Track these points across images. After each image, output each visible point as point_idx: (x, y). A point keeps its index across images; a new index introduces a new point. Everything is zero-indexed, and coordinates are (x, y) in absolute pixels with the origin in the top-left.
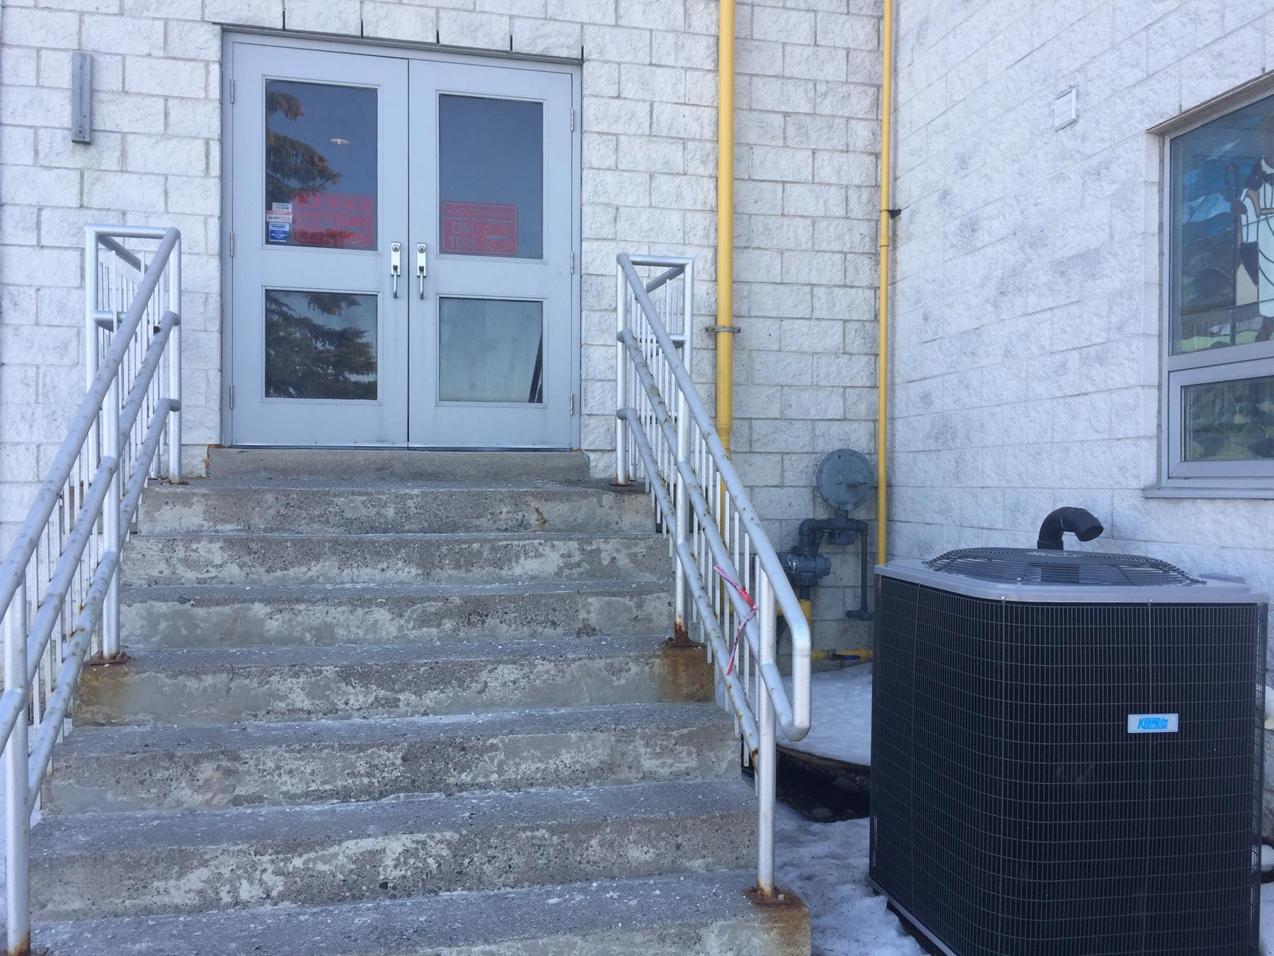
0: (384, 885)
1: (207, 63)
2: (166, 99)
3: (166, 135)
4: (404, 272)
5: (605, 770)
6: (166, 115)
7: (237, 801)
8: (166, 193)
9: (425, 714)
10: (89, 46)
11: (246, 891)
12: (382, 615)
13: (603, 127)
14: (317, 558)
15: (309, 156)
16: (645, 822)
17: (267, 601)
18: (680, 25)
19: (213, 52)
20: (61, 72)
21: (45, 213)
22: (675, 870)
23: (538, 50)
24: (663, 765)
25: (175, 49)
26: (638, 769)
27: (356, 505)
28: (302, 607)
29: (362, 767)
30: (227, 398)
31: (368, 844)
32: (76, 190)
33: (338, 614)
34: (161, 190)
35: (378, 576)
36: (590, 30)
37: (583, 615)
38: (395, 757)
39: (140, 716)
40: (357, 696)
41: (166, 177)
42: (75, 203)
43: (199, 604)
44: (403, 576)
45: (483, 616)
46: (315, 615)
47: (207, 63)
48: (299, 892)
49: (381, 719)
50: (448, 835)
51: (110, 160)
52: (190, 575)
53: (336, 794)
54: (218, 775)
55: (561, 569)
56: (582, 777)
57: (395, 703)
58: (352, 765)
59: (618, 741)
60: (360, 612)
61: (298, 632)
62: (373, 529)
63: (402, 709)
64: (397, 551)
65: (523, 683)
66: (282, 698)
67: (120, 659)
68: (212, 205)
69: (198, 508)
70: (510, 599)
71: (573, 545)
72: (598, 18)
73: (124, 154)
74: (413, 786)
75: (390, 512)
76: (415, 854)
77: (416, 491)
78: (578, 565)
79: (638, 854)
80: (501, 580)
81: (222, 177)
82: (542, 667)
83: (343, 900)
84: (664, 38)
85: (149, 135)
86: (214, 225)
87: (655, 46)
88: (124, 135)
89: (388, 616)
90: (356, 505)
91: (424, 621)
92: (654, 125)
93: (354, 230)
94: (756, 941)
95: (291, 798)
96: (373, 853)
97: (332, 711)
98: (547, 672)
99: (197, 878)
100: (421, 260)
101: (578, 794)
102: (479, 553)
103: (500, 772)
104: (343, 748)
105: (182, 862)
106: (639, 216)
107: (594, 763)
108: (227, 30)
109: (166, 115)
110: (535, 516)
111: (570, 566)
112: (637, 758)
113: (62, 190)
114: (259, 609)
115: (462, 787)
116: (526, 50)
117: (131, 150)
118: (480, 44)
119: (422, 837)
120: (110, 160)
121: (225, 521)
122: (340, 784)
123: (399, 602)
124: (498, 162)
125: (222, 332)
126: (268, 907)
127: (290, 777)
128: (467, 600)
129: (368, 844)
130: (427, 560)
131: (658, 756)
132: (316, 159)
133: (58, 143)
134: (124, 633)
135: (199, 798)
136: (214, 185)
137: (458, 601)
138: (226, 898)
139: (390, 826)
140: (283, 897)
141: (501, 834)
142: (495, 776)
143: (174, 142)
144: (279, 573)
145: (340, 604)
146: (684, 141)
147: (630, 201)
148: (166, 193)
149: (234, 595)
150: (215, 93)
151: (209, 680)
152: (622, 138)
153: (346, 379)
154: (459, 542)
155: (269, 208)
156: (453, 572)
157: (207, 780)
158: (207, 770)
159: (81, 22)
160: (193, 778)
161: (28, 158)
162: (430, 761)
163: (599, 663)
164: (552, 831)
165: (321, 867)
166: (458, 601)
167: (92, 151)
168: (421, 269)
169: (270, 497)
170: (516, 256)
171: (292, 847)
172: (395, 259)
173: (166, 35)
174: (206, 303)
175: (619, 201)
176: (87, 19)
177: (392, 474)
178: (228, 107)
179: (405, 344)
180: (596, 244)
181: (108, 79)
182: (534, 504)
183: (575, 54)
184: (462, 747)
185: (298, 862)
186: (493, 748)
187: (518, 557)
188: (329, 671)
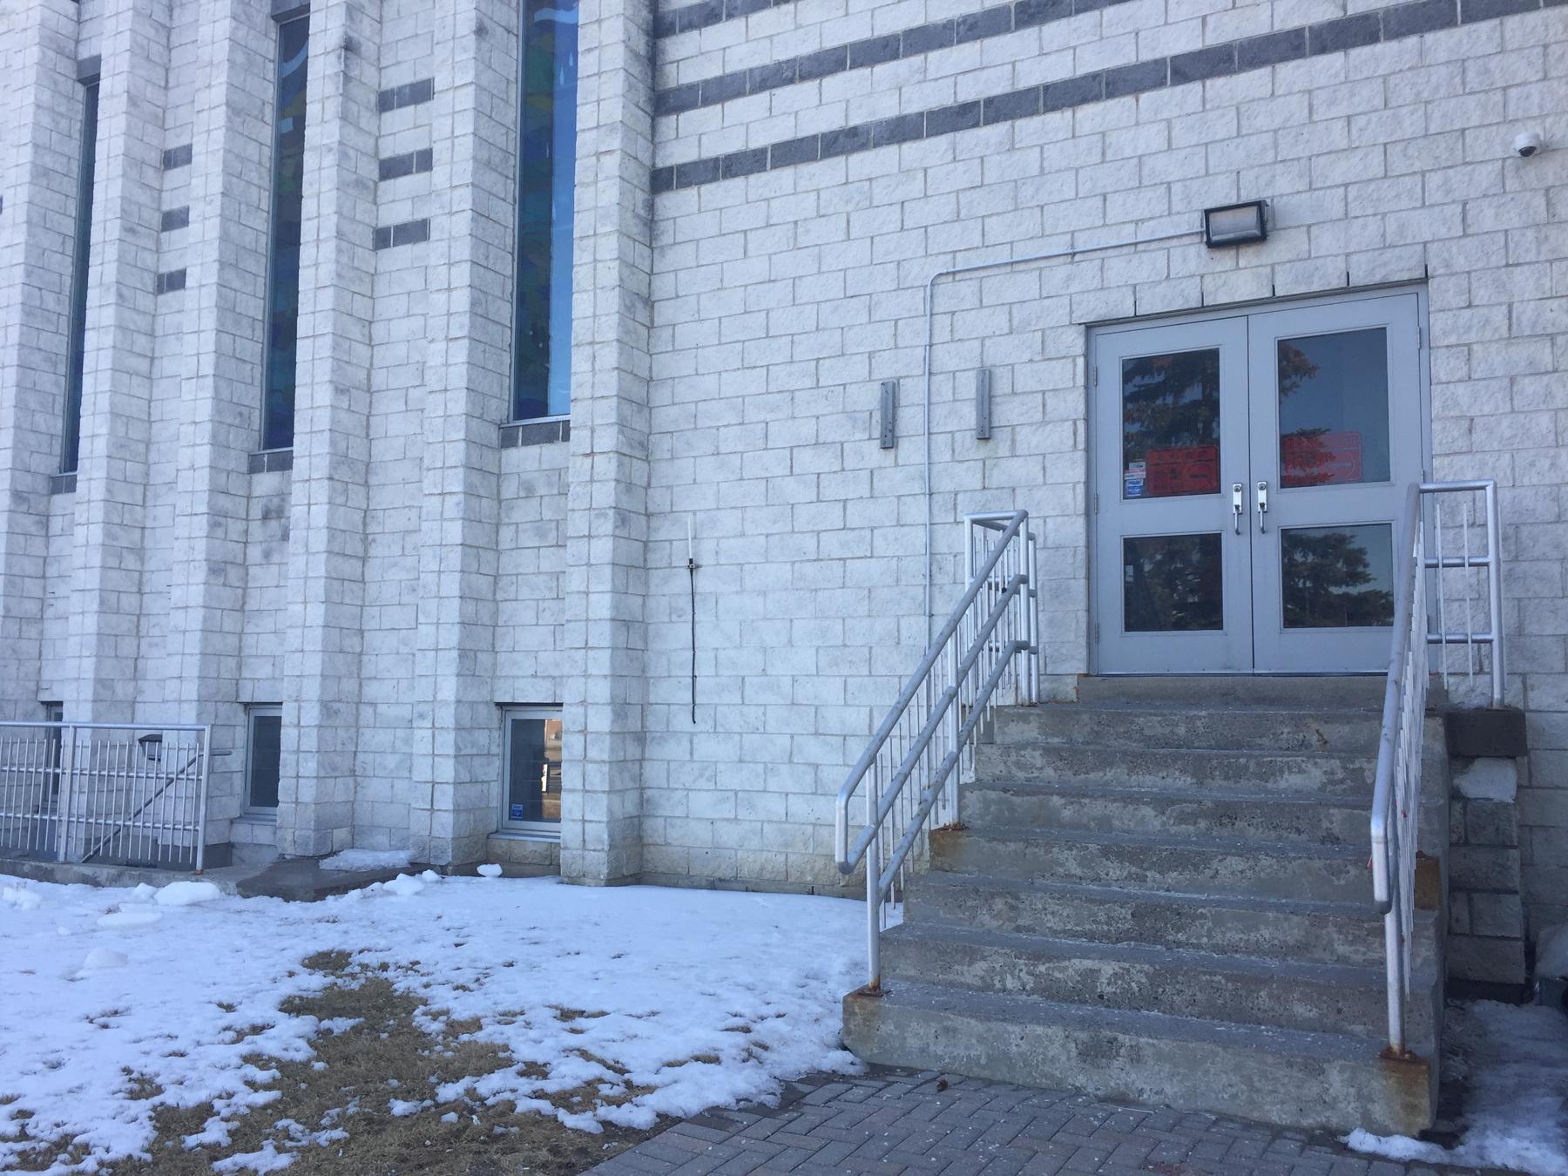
0: (1101, 997)
1: (1074, 358)
2: (1044, 392)
3: (1044, 422)
4: (1244, 512)
5: (1301, 948)
6: (1044, 406)
7: (1018, 929)
8: (1044, 468)
9: (1168, 890)
10: (988, 363)
11: (1010, 983)
12: (1148, 811)
13: (1453, 340)
14: (1111, 765)
15: (1168, 413)
16: (1307, 984)
17: (1062, 794)
18: (1542, 215)
19: (1079, 348)
20: (969, 387)
21: (960, 497)
22: (1336, 1030)
23: (1377, 279)
24: (1356, 952)
25: (1051, 352)
26: (1333, 952)
27: (1152, 724)
28: (1087, 801)
29: (1102, 918)
30: (1093, 634)
31: (1089, 964)
32: (979, 476)
33: (1114, 808)
34: (1039, 467)
35: (1160, 783)
36: (1433, 248)
37: (1325, 824)
38: (1126, 912)
39: (970, 868)
40: (1114, 870)
41: (1044, 455)
42: (979, 486)
43: (1016, 794)
44: (1179, 784)
45: (1233, 819)
46: (1097, 808)
47: (1074, 358)
48: (1044, 990)
49: (1133, 889)
50: (1146, 967)
51: (1003, 450)
52: (1021, 775)
53: (1084, 934)
54: (1006, 908)
55: (1324, 785)
56: (1274, 951)
57: (1143, 879)
58: (1095, 914)
59: (1312, 925)
60: (1131, 808)
61: (1085, 821)
62: (1167, 745)
63: (1150, 884)
64: (1174, 761)
65: (1249, 873)
66: (1062, 865)
67: (959, 827)
68: (1079, 473)
69: (1034, 724)
70: (1256, 805)
71: (1335, 763)
72: (1443, 233)
73: (1013, 441)
74: (1140, 938)
75: (1182, 730)
76: (1122, 977)
77: (1203, 713)
78: (1342, 782)
79: (1301, 1010)
80: (1267, 792)
81: (1087, 450)
82: (1265, 861)
83: (1073, 1002)
84: (1523, 235)
85: (1031, 424)
86: (1081, 489)
87: (1511, 246)
88: (1013, 427)
89: (1153, 813)
90: (1152, 724)
91: (1182, 819)
92: (1514, 327)
93: (1207, 480)
94: (1374, 1084)
95: (1055, 933)
96: (1092, 971)
97: (1097, 879)
98: (1271, 866)
99: (980, 967)
100: (1262, 496)
101: (1273, 963)
102: (1246, 767)
103: (1209, 937)
104: (1088, 900)
105: (971, 955)
106: (1499, 423)
107: (1291, 942)
108: (1089, 327)
109: (1044, 406)
110: (1316, 737)
111: (1333, 783)
112: (1331, 943)
113: (968, 477)
114: (1056, 800)
115: (1179, 944)
116: (1362, 283)
117: (1018, 438)
118: (1315, 288)
119: (1127, 965)
120: (1003, 450)
121: (1053, 735)
122: (1087, 927)
123: (1162, 802)
124: (1337, 392)
125: (1088, 578)
126: (1024, 997)
127: (1055, 917)
128: (1217, 804)
129: (1089, 964)
130: (1200, 771)
131: (1351, 943)
132: (1291, 356)
133: (968, 440)
134: (965, 814)
135: (995, 923)
136: (1080, 456)
137: (1209, 804)
138: (998, 985)
139: (1104, 956)
140: (1033, 991)
141: (1186, 973)
142: (1205, 940)
143: (1049, 427)
144: (1083, 776)
145: (1115, 801)
146: (1552, 337)
147: (1486, 410)
148: (1044, 468)
149: (1046, 790)
150: (1081, 381)
151: (1012, 846)
152: (1475, 347)
153: (1328, 593)
154: (1228, 757)
155: (1126, 467)
156: (1224, 783)
157: (1000, 912)
158: (999, 904)
159: (983, 345)
160: (990, 909)
161: (948, 457)
162: (1152, 922)
163: (1317, 864)
164: (1228, 978)
165: (1057, 975)
166: (1209, 804)
167: (991, 443)
168: (1262, 505)
169: (1086, 717)
170: (1361, 480)
171: (1037, 957)
172: (1237, 499)
173: (1043, 342)
174: (1074, 555)
175: (1474, 412)
176: (987, 342)
177: (1237, 699)
178: (1093, 391)
179: (1252, 579)
180: (1447, 460)
181: (1002, 386)
182: (1315, 726)
183: (1419, 274)
184: (1180, 914)
185: (1042, 968)
186: (1203, 916)
187: (1282, 772)
188: (1093, 847)
